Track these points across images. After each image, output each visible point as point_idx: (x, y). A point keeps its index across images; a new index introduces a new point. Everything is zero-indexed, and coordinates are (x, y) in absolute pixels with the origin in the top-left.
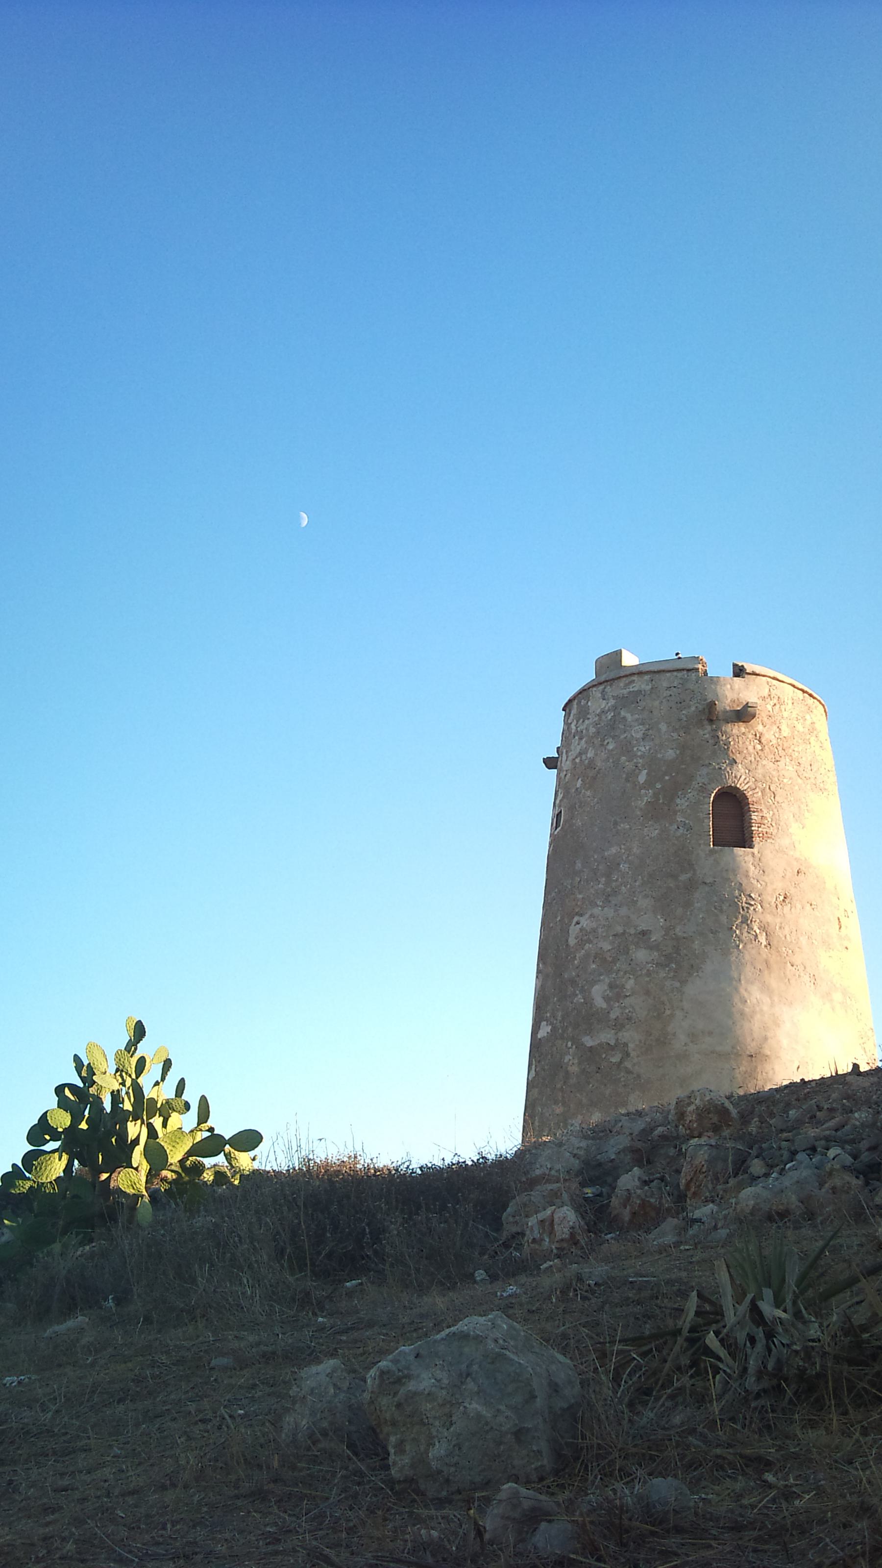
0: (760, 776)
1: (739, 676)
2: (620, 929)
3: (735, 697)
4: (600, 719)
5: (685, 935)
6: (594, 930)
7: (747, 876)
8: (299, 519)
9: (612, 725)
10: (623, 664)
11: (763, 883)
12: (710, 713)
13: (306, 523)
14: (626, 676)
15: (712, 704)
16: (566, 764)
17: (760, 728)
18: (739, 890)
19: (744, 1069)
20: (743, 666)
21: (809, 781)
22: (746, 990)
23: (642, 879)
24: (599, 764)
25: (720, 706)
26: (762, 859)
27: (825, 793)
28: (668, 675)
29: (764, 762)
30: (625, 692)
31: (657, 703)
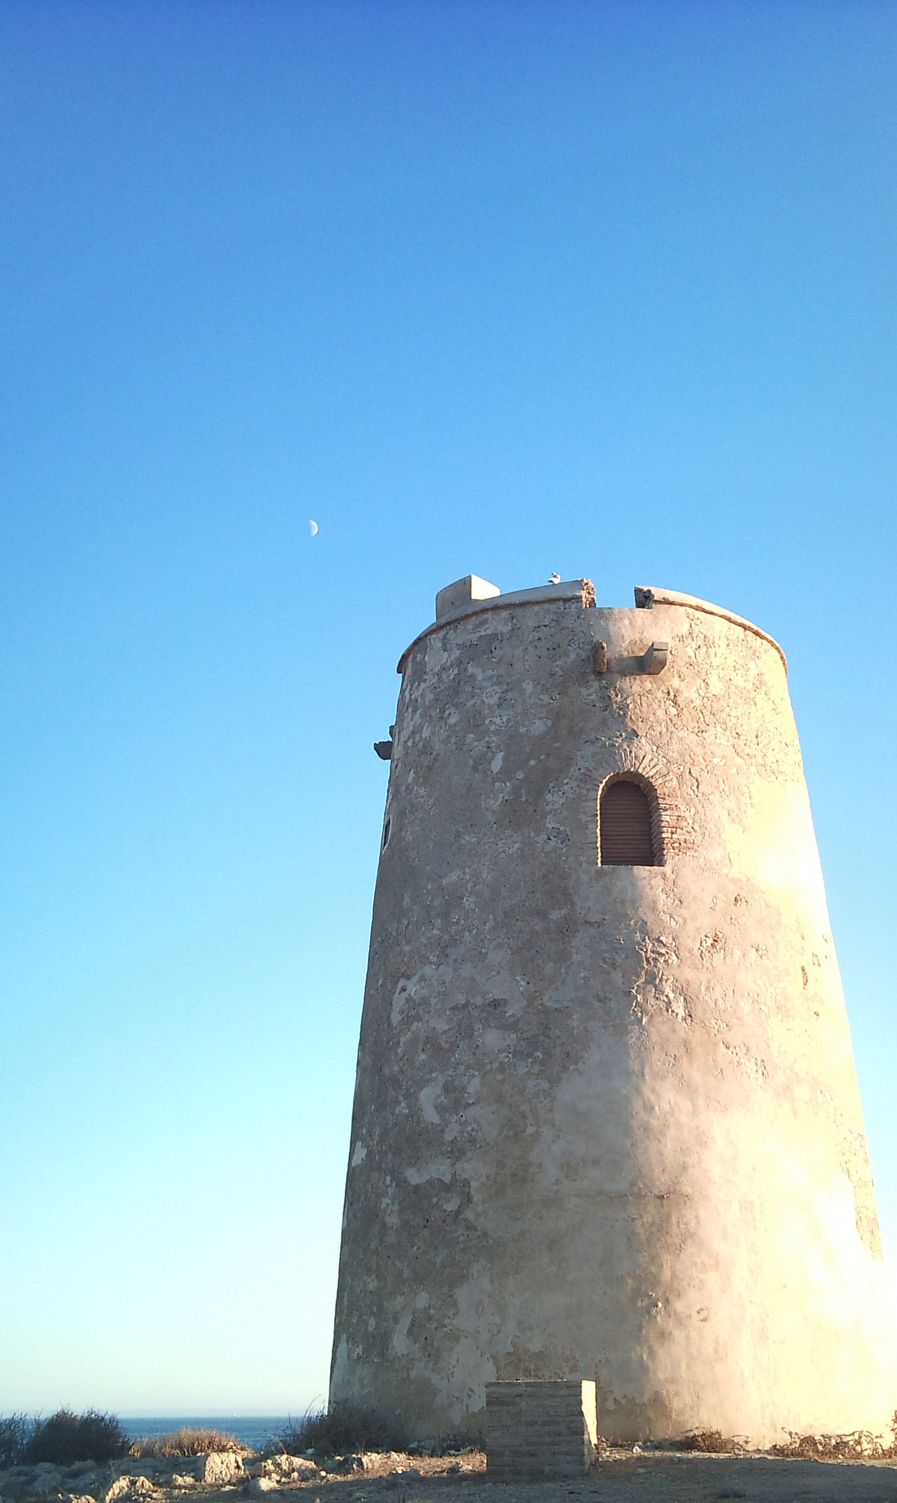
0: (675, 755)
1: (643, 607)
2: (461, 999)
3: (637, 637)
4: (440, 680)
5: (557, 1006)
6: (425, 1001)
7: (654, 910)
8: (309, 528)
9: (456, 688)
10: (474, 596)
11: (681, 920)
12: (595, 661)
13: (316, 531)
14: (475, 614)
15: (597, 649)
16: (397, 751)
17: (676, 682)
18: (641, 932)
19: (650, 1219)
20: (649, 591)
21: (754, 761)
22: (653, 1090)
23: (495, 919)
24: (437, 746)
25: (609, 653)
26: (679, 882)
27: (781, 778)
29: (681, 734)
30: (474, 637)
31: (518, 652)
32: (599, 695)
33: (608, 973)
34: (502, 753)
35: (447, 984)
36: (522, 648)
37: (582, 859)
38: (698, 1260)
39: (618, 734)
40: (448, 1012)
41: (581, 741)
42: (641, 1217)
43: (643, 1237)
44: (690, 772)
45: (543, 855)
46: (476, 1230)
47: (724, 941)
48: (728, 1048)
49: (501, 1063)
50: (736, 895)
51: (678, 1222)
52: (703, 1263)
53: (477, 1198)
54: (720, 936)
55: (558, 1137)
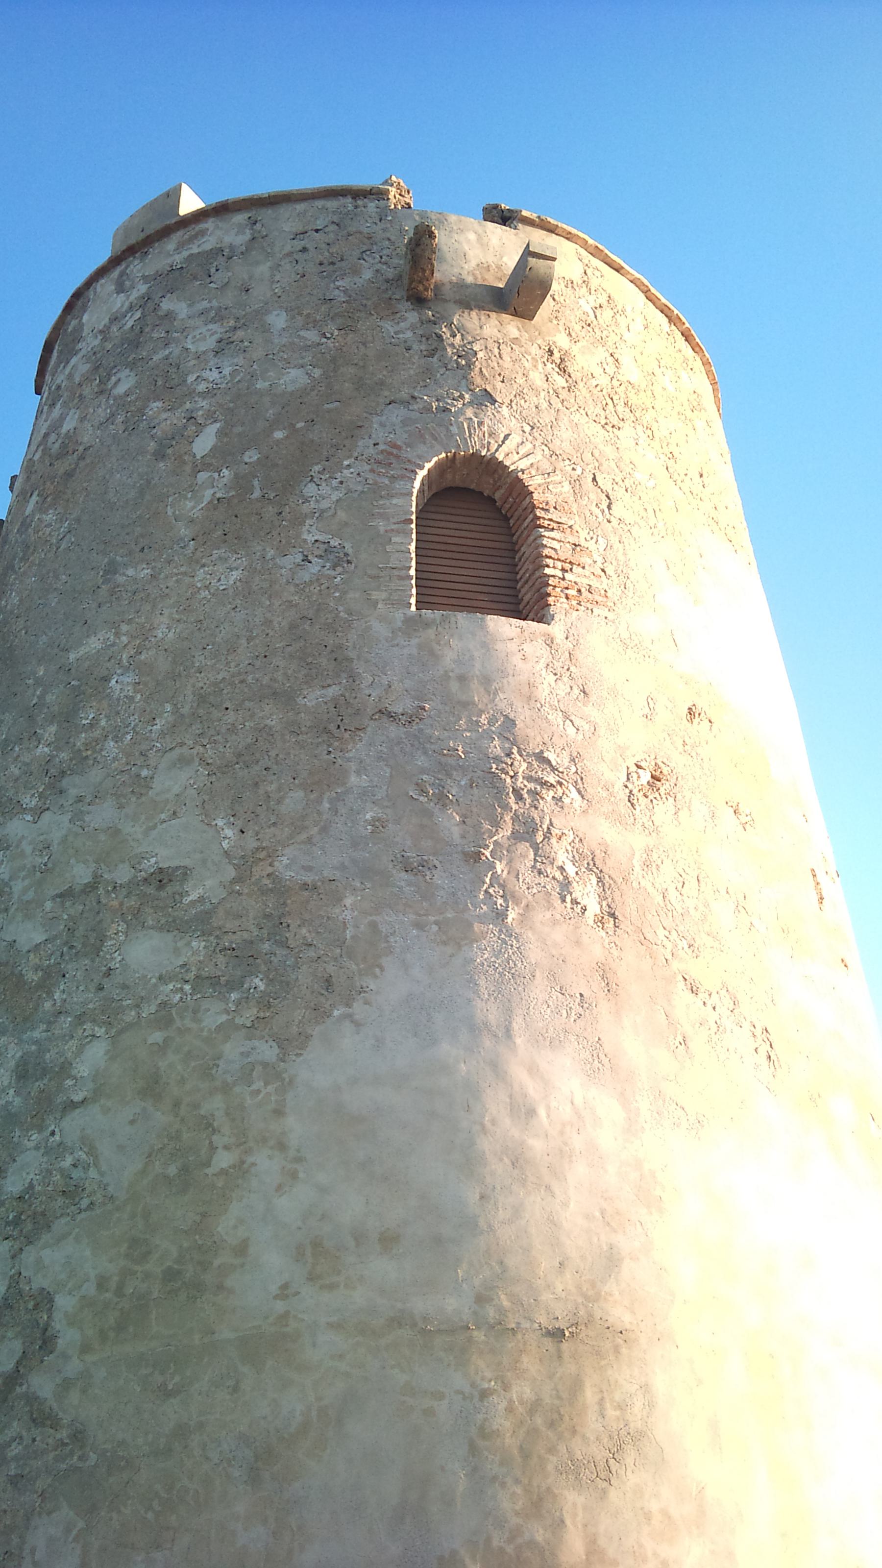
2: (81, 874)
3: (491, 259)
5: (309, 878)
9: (134, 340)
17: (562, 341)
19: (528, 1393)
22: (533, 1070)
23: (176, 710)
26: (579, 655)
28: (300, 207)
29: (576, 417)
31: (263, 269)
32: (420, 332)
33: (429, 814)
34: (218, 425)
35: (55, 848)
36: (268, 264)
37: (375, 595)
38: (654, 1506)
39: (457, 394)
40: (49, 905)
41: (381, 400)
42: (506, 1387)
43: (510, 1441)
44: (594, 479)
45: (292, 589)
46: (55, 1425)
47: (673, 781)
48: (694, 991)
49: (163, 1005)
50: (690, 705)
51: (601, 1402)
52: (665, 1513)
53: (67, 1337)
54: (665, 770)
55: (294, 1175)
